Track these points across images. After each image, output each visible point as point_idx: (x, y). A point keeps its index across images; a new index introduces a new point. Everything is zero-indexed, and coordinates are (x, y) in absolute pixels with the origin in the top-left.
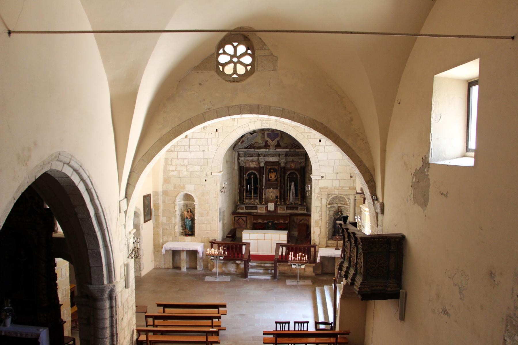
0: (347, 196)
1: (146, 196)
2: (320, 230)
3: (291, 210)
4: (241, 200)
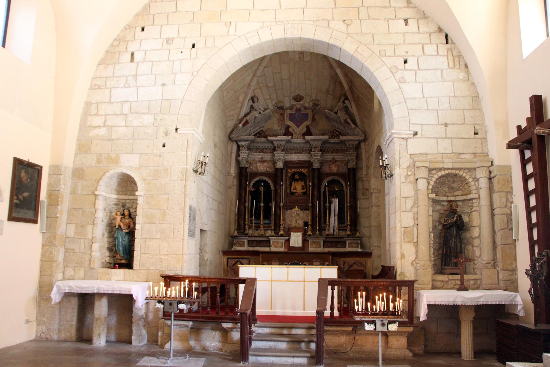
0: (470, 174)
1: (26, 163)
2: (417, 252)
3: (332, 247)
4: (241, 228)
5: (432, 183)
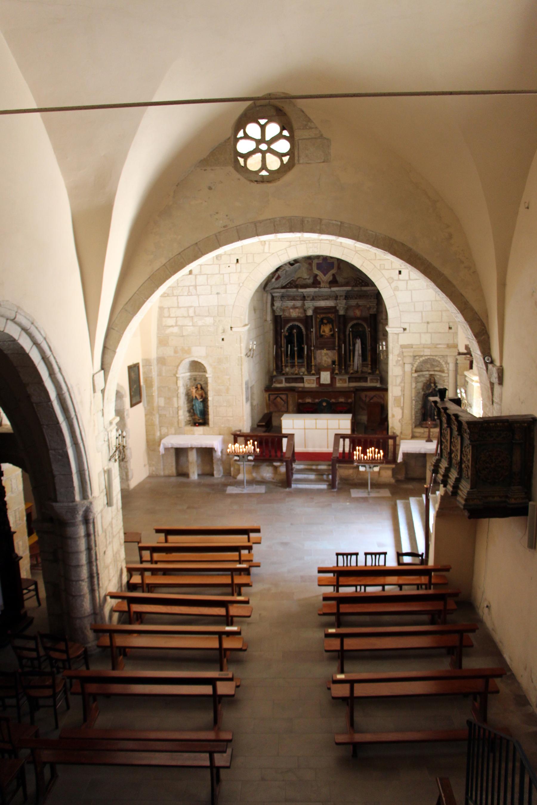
2: (403, 413)
4: (279, 369)
5: (415, 366)
